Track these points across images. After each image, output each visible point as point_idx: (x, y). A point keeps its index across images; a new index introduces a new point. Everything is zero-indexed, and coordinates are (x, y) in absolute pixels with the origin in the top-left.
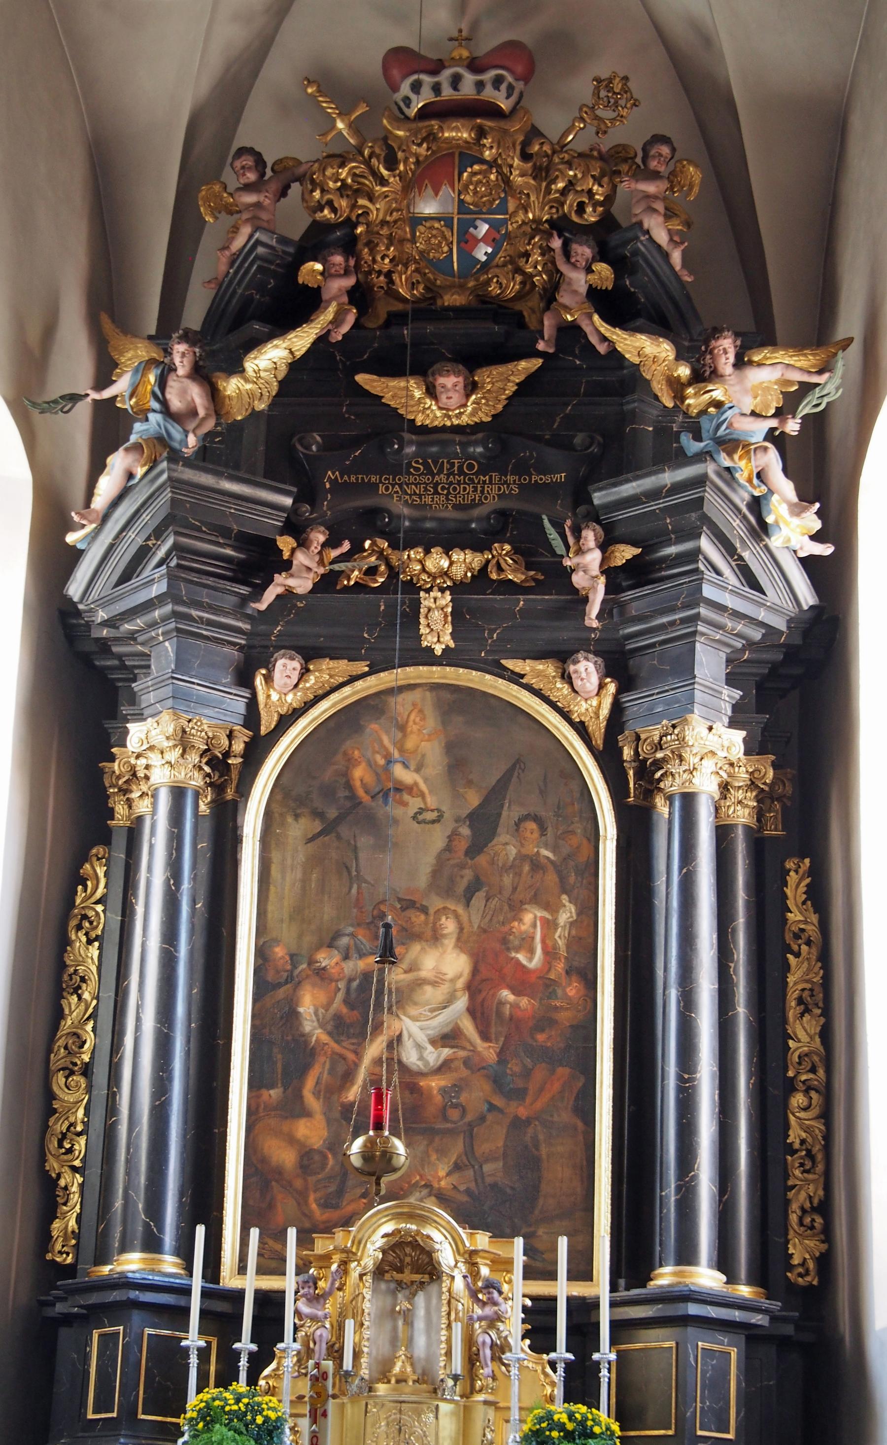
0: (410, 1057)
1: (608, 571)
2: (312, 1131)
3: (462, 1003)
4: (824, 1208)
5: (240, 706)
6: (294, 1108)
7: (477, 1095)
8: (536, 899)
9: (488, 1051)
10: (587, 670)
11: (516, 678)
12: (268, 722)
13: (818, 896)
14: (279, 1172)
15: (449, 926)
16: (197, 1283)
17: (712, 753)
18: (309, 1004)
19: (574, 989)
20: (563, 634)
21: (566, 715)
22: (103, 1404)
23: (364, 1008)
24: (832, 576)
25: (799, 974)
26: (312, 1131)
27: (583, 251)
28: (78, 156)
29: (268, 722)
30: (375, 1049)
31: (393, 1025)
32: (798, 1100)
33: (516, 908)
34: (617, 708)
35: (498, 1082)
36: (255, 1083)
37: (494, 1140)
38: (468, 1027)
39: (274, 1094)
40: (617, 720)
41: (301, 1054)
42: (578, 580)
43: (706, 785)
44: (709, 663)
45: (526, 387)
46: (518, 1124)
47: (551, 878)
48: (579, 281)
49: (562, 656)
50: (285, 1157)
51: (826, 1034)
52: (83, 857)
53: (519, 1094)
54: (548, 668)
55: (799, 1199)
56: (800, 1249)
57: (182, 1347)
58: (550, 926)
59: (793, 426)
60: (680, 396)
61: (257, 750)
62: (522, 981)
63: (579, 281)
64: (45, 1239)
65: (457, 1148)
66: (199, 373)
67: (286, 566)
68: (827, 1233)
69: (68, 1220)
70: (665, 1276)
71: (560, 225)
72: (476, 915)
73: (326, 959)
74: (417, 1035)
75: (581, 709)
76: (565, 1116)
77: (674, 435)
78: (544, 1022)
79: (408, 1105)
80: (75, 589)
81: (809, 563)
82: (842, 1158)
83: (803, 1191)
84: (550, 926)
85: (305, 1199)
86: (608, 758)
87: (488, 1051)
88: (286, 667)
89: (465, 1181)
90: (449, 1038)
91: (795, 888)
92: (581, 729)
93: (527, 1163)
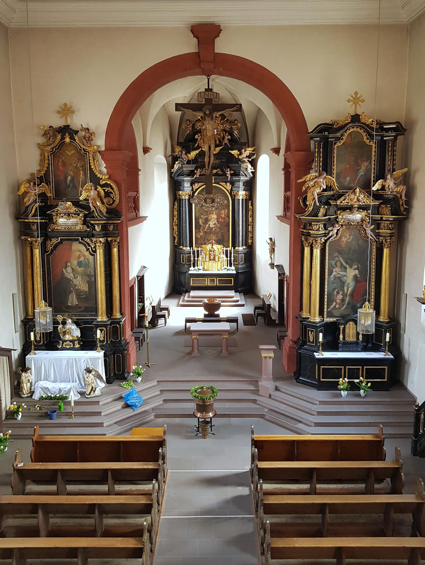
0: (211, 226)
1: (230, 174)
2: (201, 234)
3: (216, 220)
4: (252, 237)
5: (191, 188)
7: (218, 230)
8: (223, 209)
9: (219, 225)
10: (228, 184)
11: (221, 185)
12: (194, 190)
13: (252, 205)
14: (198, 238)
15: (214, 212)
16: (192, 250)
17: (242, 194)
19: (227, 219)
21: (226, 189)
23: (207, 221)
24: (254, 173)
25: (250, 213)
26: (201, 234)
29: (194, 190)
30: (207, 225)
31: (209, 223)
32: (250, 226)
33: (221, 210)
34: (231, 188)
35: (220, 229)
36: (195, 229)
37: (219, 234)
38: (217, 223)
39: (197, 230)
40: (231, 190)
41: (200, 226)
42: (227, 175)
43: (241, 198)
44: (241, 184)
46: (222, 233)
47: (225, 207)
49: (226, 182)
50: (199, 237)
51: (253, 219)
52: (174, 202)
53: (222, 230)
54: (224, 183)
55: (250, 236)
56: (250, 241)
57: (208, 312)
58: (225, 212)
59: (250, 160)
60: (238, 157)
61: (194, 193)
63: (227, 137)
64: (174, 242)
65: (216, 236)
68: (252, 240)
69: (176, 241)
70: (237, 248)
71: (224, 130)
72: (217, 211)
73: (202, 216)
74: (212, 224)
76: (227, 232)
78: (224, 222)
79: (210, 231)
80: (173, 175)
81: (252, 172)
82: (317, 560)
83: (250, 235)
84: (225, 212)
85: (201, 242)
86: (230, 193)
87: (219, 225)
88: (196, 184)
89: (217, 238)
90: (215, 224)
91: (250, 204)
92: (227, 190)
93: (223, 236)
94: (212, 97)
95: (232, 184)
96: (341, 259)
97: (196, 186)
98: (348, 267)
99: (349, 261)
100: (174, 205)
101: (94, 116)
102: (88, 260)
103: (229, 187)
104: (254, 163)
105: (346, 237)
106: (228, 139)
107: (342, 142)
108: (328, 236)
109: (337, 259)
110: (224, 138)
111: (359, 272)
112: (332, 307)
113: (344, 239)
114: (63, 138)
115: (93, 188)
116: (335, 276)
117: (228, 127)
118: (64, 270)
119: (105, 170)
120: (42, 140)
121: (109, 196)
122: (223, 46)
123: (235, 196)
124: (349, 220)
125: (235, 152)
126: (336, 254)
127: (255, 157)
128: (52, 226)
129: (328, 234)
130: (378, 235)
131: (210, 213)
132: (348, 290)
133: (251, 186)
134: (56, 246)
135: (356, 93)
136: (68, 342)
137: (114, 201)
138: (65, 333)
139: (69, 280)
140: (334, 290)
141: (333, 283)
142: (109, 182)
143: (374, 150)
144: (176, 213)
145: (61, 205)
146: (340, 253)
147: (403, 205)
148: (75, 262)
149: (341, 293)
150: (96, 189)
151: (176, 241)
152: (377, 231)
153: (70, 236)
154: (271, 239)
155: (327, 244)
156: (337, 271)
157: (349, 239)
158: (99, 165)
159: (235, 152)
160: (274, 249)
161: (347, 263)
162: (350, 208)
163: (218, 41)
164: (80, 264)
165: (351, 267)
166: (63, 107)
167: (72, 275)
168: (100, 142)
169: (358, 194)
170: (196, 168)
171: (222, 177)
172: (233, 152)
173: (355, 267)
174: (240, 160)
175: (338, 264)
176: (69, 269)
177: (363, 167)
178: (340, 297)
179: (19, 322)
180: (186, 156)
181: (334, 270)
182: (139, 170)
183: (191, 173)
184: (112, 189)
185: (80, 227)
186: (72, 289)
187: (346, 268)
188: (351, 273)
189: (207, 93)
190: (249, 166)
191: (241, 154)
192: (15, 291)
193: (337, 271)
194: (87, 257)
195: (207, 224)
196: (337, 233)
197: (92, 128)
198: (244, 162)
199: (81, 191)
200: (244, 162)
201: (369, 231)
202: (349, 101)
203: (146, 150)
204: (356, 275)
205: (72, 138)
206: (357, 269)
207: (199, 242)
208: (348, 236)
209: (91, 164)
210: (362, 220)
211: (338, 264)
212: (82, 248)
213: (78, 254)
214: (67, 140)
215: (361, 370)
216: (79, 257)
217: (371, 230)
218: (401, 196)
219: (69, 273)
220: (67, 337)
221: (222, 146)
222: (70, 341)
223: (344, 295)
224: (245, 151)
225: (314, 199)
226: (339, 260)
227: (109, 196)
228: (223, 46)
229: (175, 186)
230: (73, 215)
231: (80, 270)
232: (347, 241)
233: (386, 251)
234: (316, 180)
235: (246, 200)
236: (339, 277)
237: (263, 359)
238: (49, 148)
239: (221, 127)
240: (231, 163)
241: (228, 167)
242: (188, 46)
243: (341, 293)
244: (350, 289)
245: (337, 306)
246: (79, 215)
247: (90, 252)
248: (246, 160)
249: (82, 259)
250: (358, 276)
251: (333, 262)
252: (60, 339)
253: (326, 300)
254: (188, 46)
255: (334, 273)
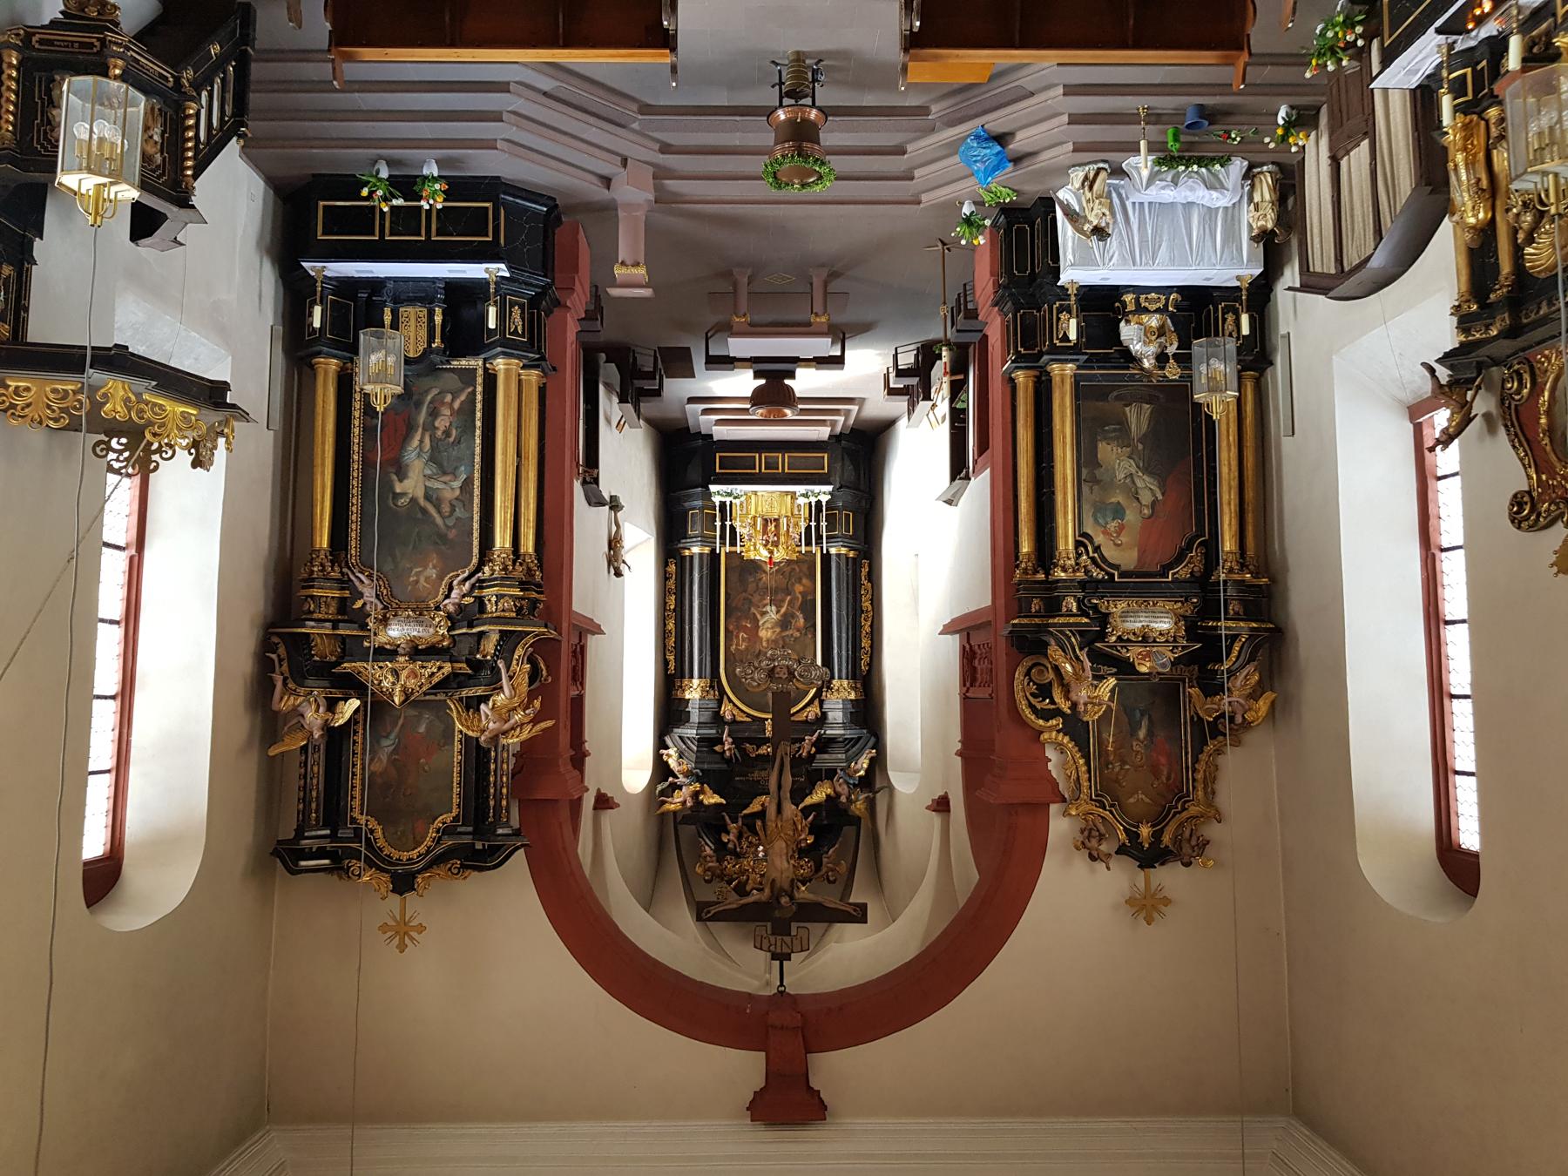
6: (803, 594)
7: (756, 598)
9: (753, 610)
10: (728, 717)
11: (748, 715)
12: (816, 702)
13: (666, 663)
17: (694, 691)
18: (801, 621)
20: (735, 727)
22: (847, 516)
23: (785, 623)
24: (660, 744)
25: (671, 642)
26: (799, 588)
27: (730, 846)
28: (886, 875)
29: (816, 702)
37: (751, 587)
41: (801, 609)
43: (696, 682)
44: (695, 717)
45: (747, 806)
48: (732, 837)
49: (734, 721)
52: (869, 671)
56: (672, 568)
61: (818, 695)
62: (745, 629)
63: (732, 837)
66: (838, 795)
67: (813, 745)
69: (865, 571)
70: (707, 550)
71: (738, 856)
74: (772, 614)
75: (730, 706)
77: (703, 777)
79: (777, 595)
80: (873, 739)
81: (667, 748)
83: (671, 584)
86: (722, 692)
87: (753, 610)
90: (764, 614)
91: (672, 666)
92: (730, 701)
93: (743, 582)
94: (772, 939)
95: (717, 719)
96: (439, 520)
97: (812, 712)
98: (422, 502)
99: (420, 516)
100: (870, 665)
101: (1075, 893)
102: (1096, 520)
103: (727, 711)
104: (661, 770)
105: (427, 579)
106: (728, 833)
107: (438, 824)
108: (473, 580)
109: (450, 522)
110: (740, 836)
111: (392, 488)
112: (463, 397)
113: (432, 573)
114: (1157, 835)
115: (1081, 708)
116: (456, 477)
117: (730, 865)
118: (1160, 497)
119: (1050, 753)
120: (1212, 831)
121: (1040, 687)
122: (744, 1069)
123: (712, 687)
124: (421, 623)
125: (711, 799)
126: (452, 534)
127: (659, 788)
128: (1188, 610)
129: (473, 587)
130: (344, 583)
131: (775, 641)
132: (421, 441)
133: (670, 713)
134: (1179, 559)
135: (402, 948)
136: (1153, 307)
137: (1028, 673)
138: (1161, 331)
139: (1147, 470)
140: (458, 442)
141: (459, 459)
142: (1041, 722)
143: (356, 803)
144: (865, 643)
145: (1164, 666)
146: (442, 537)
147: (280, 660)
148: (1131, 516)
149: (439, 433)
150: (1074, 706)
151: (865, 571)
152: (347, 594)
153: (1141, 585)
154: (618, 574)
155: (475, 560)
156: (450, 489)
157: (418, 574)
158: (1064, 765)
159: (711, 799)
160: (610, 548)
161: (424, 511)
162: (418, 652)
163: (759, 1082)
164: (1118, 512)
165: (413, 500)
166: (1155, 915)
167: (1139, 484)
168: (1060, 826)
169: (398, 688)
170: (811, 758)
171: (746, 734)
172: (716, 799)
173: (402, 501)
174: (699, 779)
175: (446, 509)
176: (1146, 498)
177: (384, 758)
178: (442, 423)
179: (1279, 360)
180: (839, 789)
181: (458, 492)
182: (959, 754)
183: (824, 745)
184: (1031, 706)
185: (1118, 607)
186: (1140, 447)
187: (427, 497)
188: (412, 485)
189: (786, 950)
190: (673, 763)
191: (695, 795)
192: (1287, 442)
193: (450, 489)
194: (1100, 529)
195: (785, 615)
196: (451, 588)
197: (1080, 861)
198: (687, 774)
199: (1111, 699)
200: (687, 774)
201: (369, 593)
202: (421, 929)
203: (942, 805)
204: (401, 481)
205: (1133, 836)
206: (396, 496)
207: (805, 568)
208: (422, 580)
209: (1084, 769)
210: (384, 621)
211: (446, 509)
212: (1110, 553)
213: (1124, 539)
214: (1145, 831)
215: (387, 231)
216: (1121, 528)
217: (361, 595)
218: (285, 684)
219: (1148, 488)
220: (1154, 321)
221: (746, 816)
222: (1146, 311)
223: (430, 427)
224: (684, 803)
225: (511, 678)
226: (443, 518)
227: (1040, 687)
228: (744, 1069)
229: (868, 712)
230: (1132, 638)
231: (1118, 498)
232: (425, 568)
233: (323, 540)
234: (506, 726)
235: (683, 677)
236: (445, 473)
237: (642, 260)
238: (1193, 810)
239: (747, 863)
240: (721, 771)
241: (729, 761)
242: (833, 1069)
243: (439, 433)
244: (416, 442)
245: (449, 398)
246: (1120, 639)
247: (1092, 542)
248: (682, 779)
249: (1113, 525)
250: (394, 477)
251: (459, 512)
252: (1172, 316)
253: (479, 415)
254: (833, 1069)
255: (457, 484)
